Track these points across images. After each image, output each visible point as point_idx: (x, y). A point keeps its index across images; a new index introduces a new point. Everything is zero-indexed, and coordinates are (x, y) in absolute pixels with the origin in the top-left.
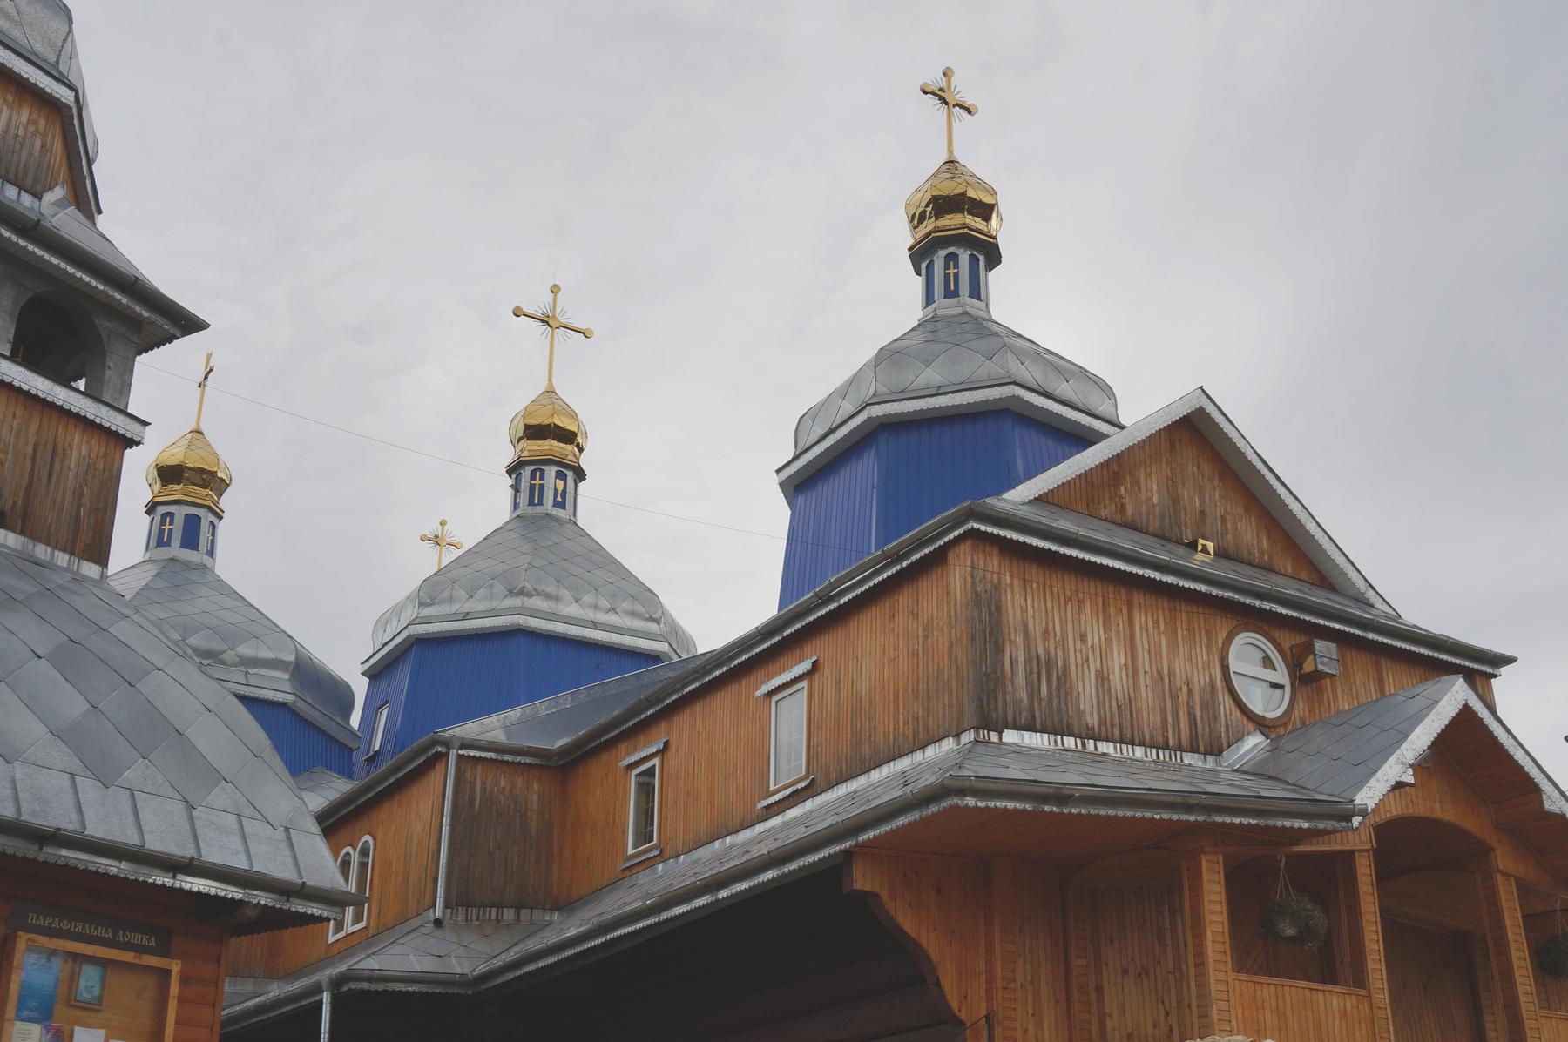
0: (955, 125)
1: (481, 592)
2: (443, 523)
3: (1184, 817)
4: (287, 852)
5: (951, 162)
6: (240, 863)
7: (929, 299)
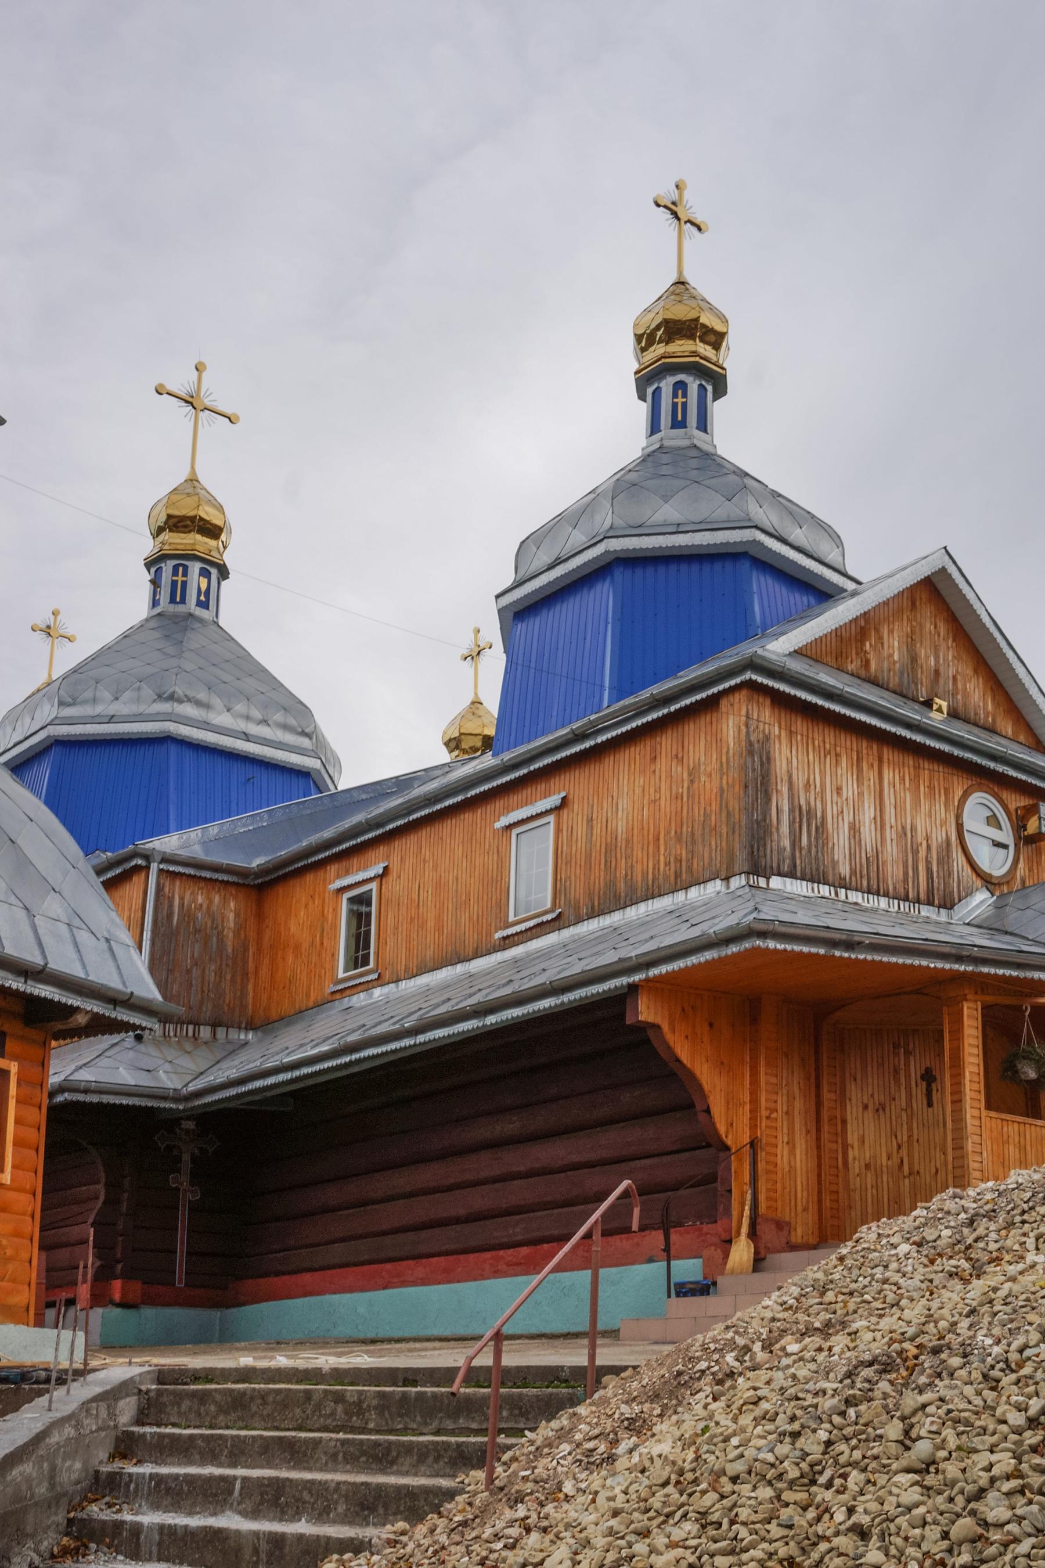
0: (687, 244)
1: (127, 695)
2: (55, 613)
3: (956, 967)
4: (110, 962)
5: (681, 283)
6: (76, 971)
7: (654, 427)
